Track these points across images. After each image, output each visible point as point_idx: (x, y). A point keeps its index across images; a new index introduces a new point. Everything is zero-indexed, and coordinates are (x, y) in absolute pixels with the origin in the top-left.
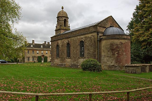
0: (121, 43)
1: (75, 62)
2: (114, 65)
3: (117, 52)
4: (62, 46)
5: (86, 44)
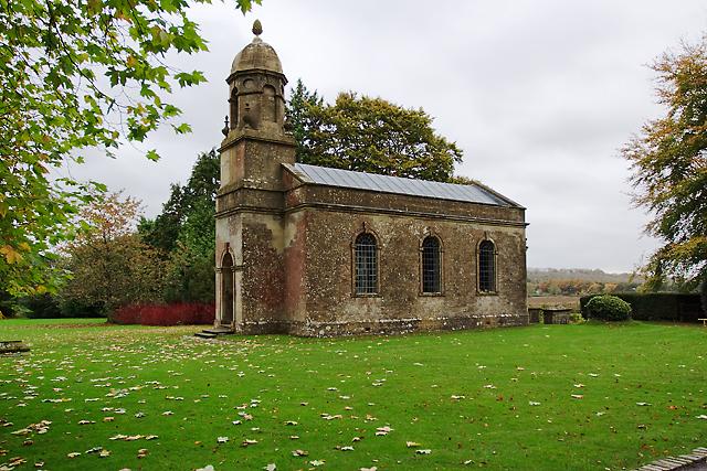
1: (462, 310)
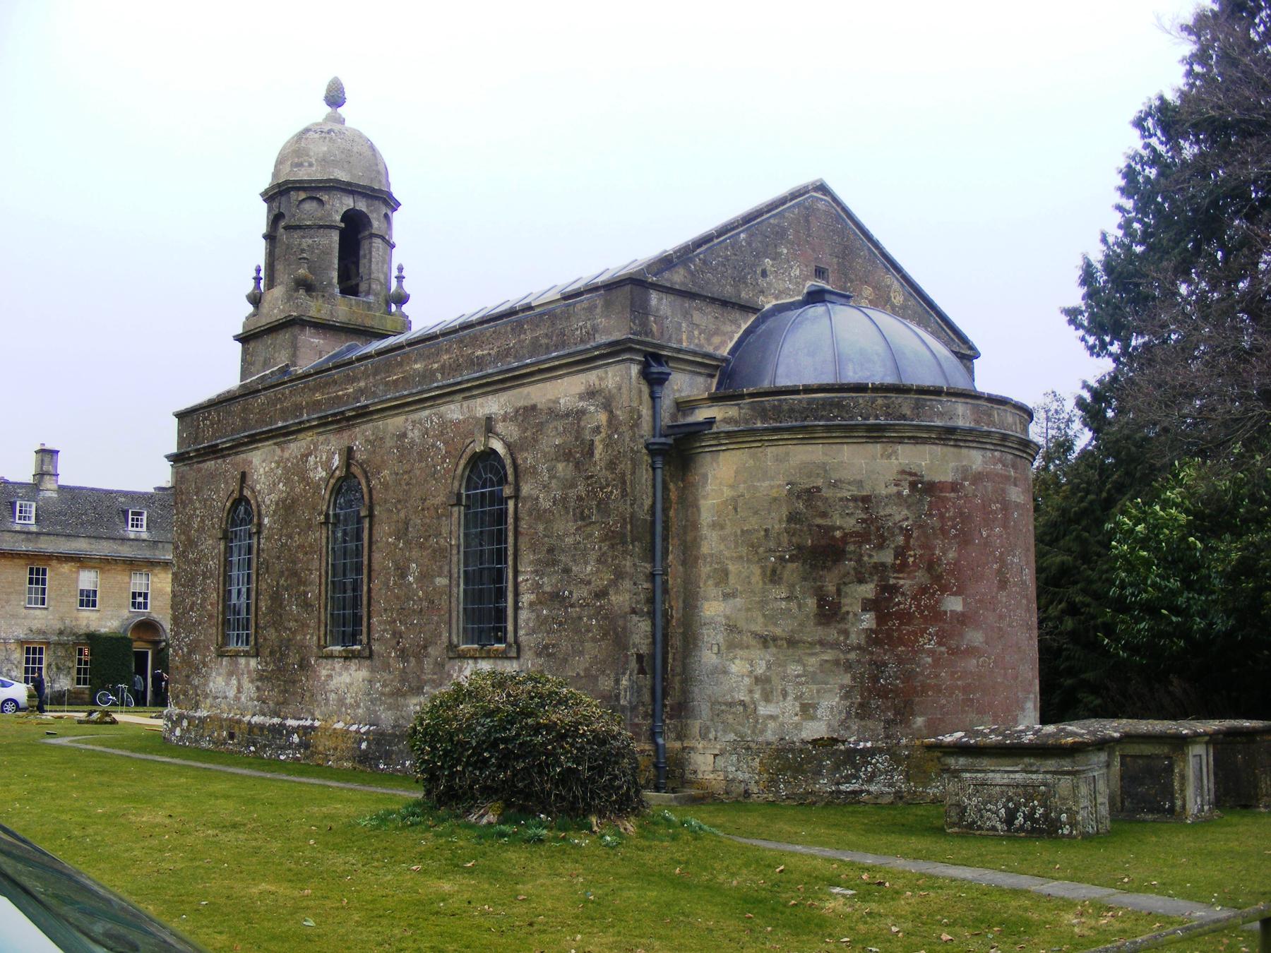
0: (913, 485)
2: (834, 741)
3: (868, 590)
4: (288, 507)
5: (526, 489)
